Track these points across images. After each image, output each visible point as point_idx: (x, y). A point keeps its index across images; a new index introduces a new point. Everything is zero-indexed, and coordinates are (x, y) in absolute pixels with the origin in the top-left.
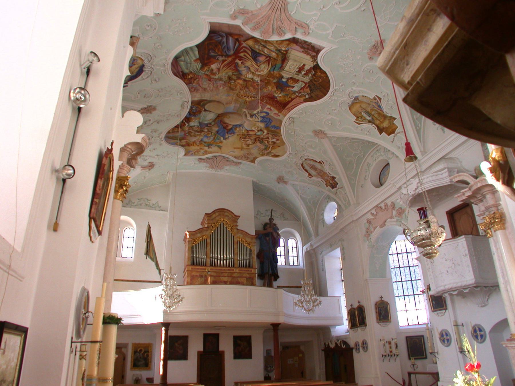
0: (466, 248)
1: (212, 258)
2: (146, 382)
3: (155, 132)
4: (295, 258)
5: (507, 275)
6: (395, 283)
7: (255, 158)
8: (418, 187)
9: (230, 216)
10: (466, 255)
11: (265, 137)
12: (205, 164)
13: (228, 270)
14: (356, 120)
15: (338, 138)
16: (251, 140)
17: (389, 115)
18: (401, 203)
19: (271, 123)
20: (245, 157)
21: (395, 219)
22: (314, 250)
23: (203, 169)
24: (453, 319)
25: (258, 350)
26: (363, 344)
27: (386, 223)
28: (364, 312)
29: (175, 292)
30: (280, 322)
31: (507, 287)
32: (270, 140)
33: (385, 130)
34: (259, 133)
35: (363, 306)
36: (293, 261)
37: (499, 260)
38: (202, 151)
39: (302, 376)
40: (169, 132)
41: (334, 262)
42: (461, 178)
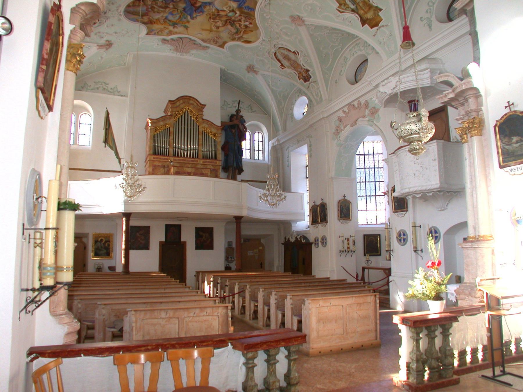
0: (436, 153)
1: (176, 148)
2: (109, 271)
3: (113, 4)
4: (261, 153)
5: (475, 181)
6: (359, 183)
7: (225, 43)
8: (396, 86)
9: (195, 104)
10: (435, 160)
11: (237, 19)
12: (169, 46)
13: (192, 161)
14: (339, 7)
15: (316, 26)
16: (221, 21)
17: (375, 5)
18: (377, 101)
19: (244, 3)
20: (214, 41)
21: (367, 119)
22: (280, 145)
23: (167, 52)
24: (412, 221)
25: (220, 241)
26: (323, 240)
27: (357, 122)
28: (327, 209)
29: (136, 181)
30: (243, 215)
31: (472, 192)
32: (243, 23)
33: (367, 22)
34: (231, 14)
35: (326, 204)
36: (258, 156)
37: (470, 166)
38: (166, 31)
39: (261, 267)
40: (129, 6)
41: (300, 159)
42: (445, 79)
